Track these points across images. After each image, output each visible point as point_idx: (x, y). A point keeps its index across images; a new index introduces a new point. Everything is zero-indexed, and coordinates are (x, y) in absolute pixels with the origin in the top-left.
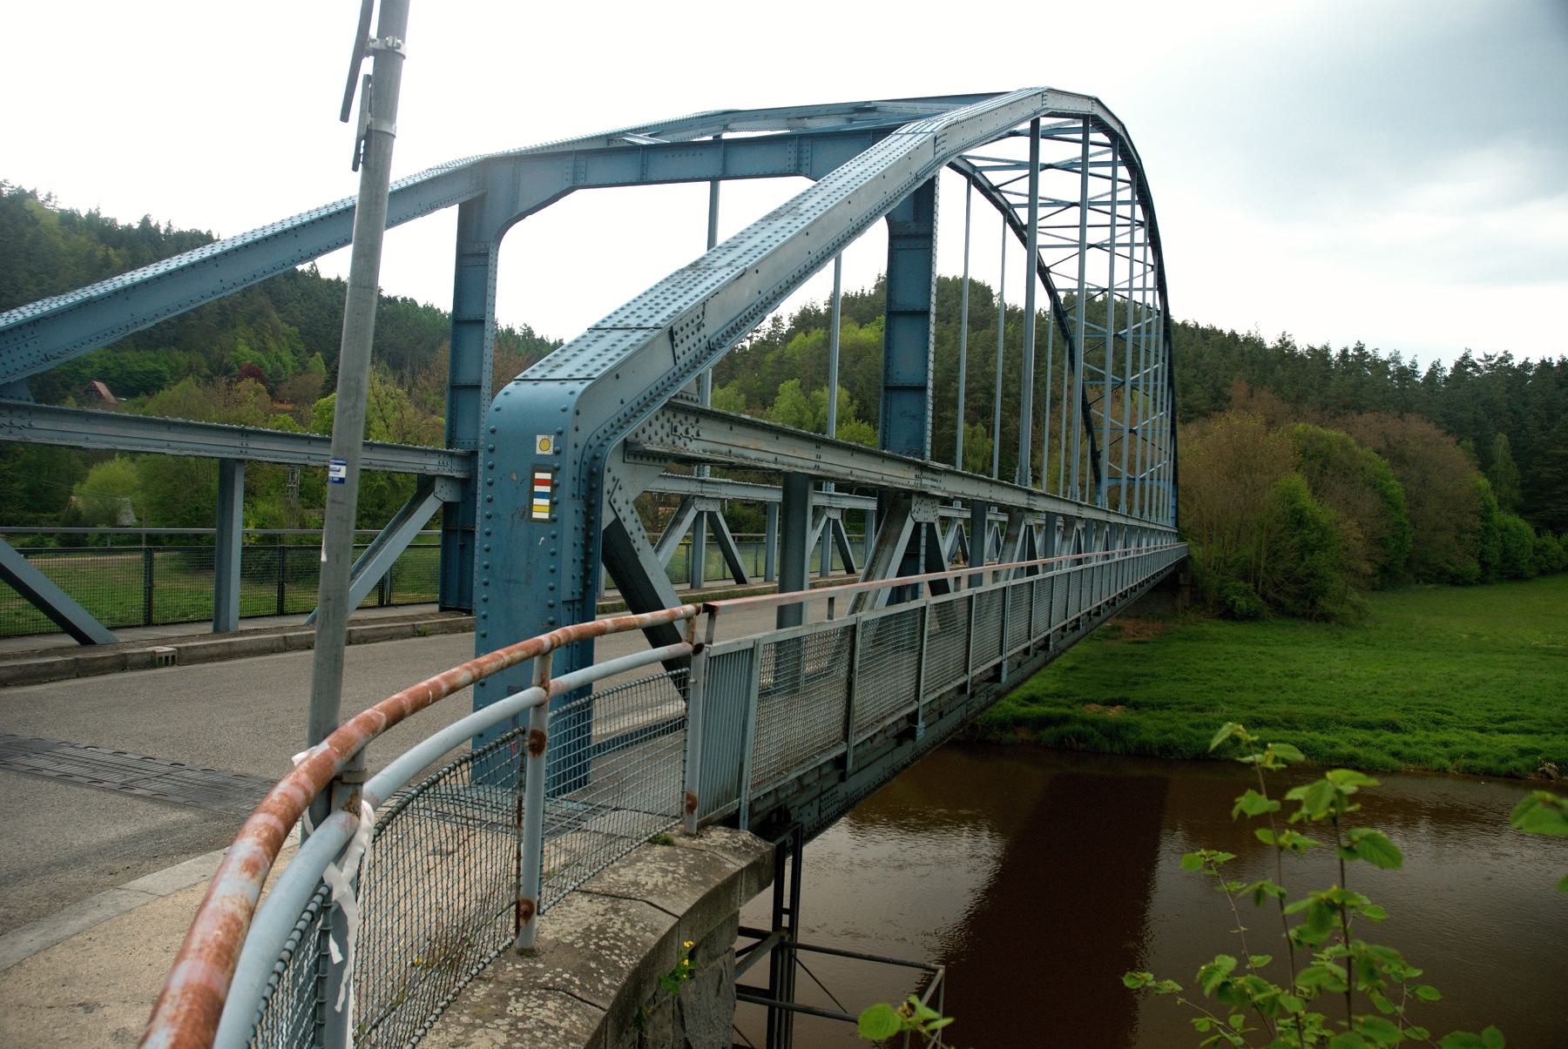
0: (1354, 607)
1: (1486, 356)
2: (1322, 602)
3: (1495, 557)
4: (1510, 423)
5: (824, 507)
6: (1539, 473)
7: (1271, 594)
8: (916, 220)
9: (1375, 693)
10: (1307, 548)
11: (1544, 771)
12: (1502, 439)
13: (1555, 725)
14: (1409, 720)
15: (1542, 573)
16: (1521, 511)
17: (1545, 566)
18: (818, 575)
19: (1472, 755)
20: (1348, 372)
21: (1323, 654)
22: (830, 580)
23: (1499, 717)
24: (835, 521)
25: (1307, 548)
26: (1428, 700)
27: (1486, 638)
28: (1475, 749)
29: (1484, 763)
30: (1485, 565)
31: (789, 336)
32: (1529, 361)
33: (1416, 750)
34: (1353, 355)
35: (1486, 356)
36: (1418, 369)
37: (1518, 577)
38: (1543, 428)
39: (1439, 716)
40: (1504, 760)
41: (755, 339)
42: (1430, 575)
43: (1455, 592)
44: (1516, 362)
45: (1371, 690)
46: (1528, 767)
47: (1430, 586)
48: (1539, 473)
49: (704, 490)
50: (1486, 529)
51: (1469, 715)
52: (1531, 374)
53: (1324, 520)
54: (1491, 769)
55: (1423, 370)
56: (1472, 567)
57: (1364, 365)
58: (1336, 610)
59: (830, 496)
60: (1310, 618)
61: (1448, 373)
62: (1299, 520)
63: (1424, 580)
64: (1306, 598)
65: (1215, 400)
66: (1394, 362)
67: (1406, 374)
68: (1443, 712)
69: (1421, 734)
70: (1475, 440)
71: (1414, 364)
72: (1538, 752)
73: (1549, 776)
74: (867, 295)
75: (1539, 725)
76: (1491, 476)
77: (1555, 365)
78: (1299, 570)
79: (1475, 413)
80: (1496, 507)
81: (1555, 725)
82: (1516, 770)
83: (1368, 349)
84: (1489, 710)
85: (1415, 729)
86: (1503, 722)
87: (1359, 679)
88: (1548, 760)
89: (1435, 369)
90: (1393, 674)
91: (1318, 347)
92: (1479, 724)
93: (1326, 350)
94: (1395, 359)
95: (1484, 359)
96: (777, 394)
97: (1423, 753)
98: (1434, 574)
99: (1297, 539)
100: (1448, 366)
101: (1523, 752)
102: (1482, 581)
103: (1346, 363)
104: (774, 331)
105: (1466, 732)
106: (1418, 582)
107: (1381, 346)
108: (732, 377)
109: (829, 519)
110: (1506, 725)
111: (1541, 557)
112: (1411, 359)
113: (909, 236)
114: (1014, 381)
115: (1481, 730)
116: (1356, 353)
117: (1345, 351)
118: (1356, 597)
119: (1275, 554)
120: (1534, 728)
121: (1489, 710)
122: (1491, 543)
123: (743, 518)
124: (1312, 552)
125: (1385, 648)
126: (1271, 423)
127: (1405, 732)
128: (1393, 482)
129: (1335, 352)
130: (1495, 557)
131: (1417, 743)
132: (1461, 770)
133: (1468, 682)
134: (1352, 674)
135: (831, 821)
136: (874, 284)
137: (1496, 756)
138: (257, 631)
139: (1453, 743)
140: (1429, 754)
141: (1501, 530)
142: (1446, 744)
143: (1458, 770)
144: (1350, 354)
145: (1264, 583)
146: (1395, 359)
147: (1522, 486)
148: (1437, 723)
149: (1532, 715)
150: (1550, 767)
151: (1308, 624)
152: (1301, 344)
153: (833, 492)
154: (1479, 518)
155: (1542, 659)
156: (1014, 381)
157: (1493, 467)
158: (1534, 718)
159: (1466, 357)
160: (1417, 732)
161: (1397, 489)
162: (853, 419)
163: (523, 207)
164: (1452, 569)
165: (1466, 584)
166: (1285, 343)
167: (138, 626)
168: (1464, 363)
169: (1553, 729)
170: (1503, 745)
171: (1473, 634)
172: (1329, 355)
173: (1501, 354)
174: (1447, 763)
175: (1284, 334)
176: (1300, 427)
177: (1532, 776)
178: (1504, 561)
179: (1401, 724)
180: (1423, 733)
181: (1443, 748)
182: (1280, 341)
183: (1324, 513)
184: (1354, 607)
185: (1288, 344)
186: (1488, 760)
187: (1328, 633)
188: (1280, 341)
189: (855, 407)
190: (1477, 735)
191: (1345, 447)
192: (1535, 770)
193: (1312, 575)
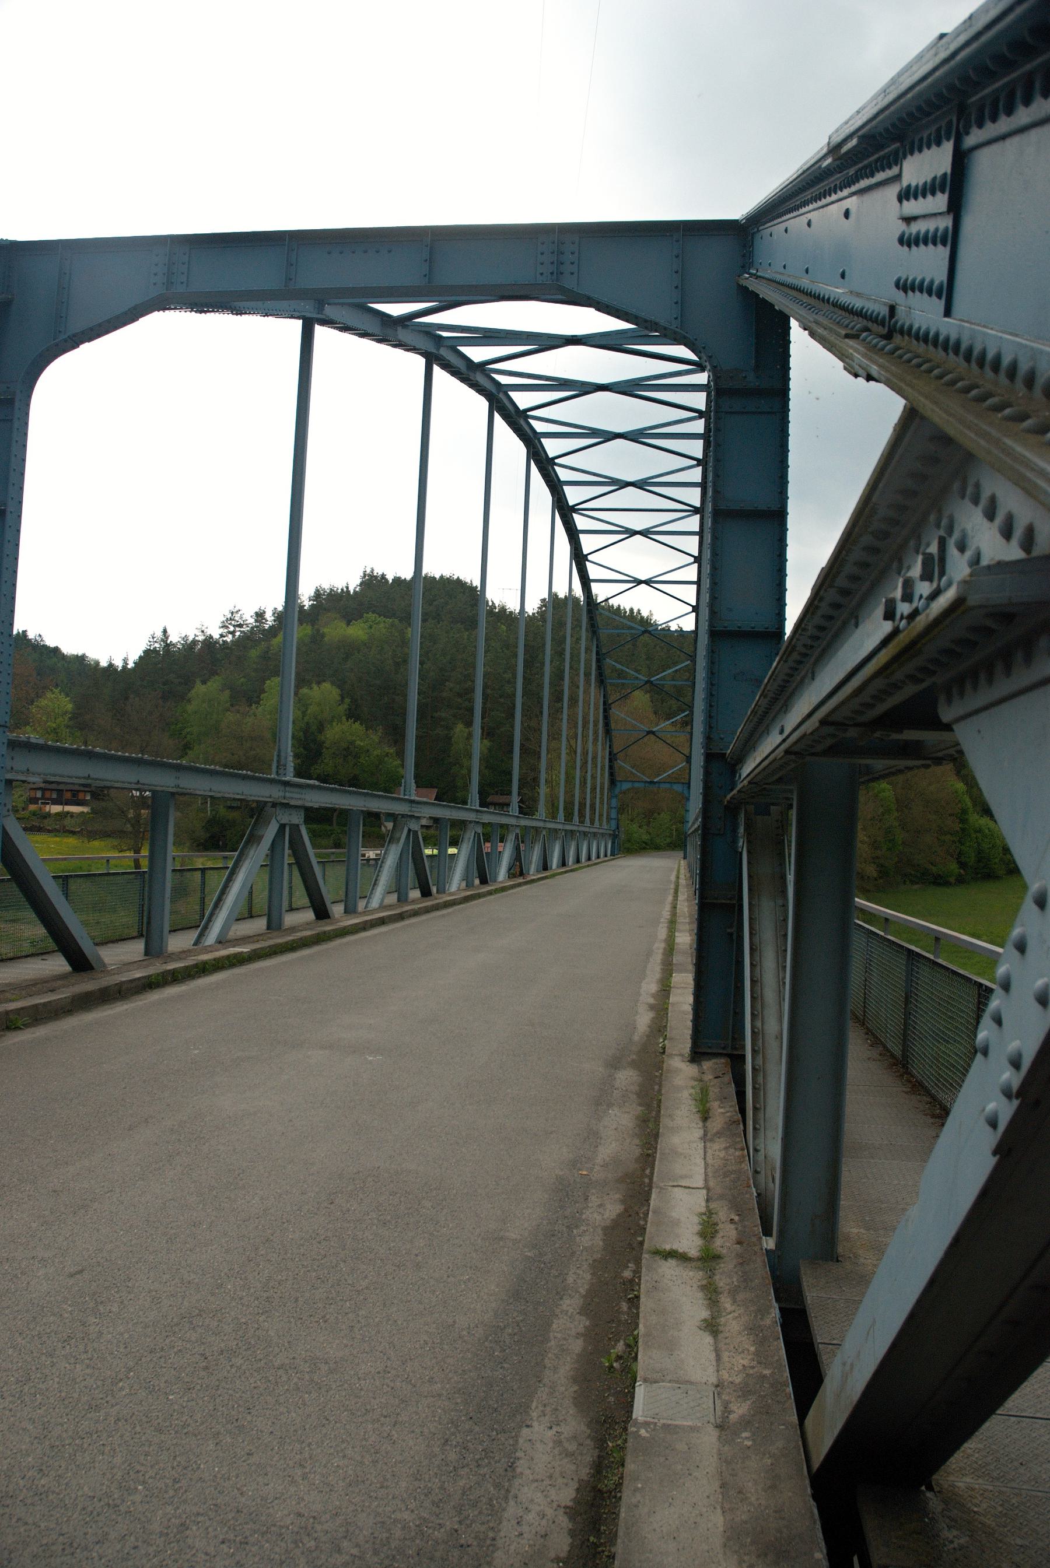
18: (259, 925)
24: (295, 828)
31: (273, 631)
41: (238, 634)
47: (916, 887)
49: (288, 795)
50: (963, 830)
74: (352, 592)
96: (263, 691)
102: (960, 881)
104: (256, 627)
108: (214, 673)
109: (409, 830)
114: (509, 682)
122: (968, 844)
123: (228, 821)
136: (359, 581)
138: (790, 855)
141: (976, 832)
153: (290, 777)
156: (509, 682)
162: (344, 718)
163: (77, 325)
164: (934, 869)
165: (947, 884)
167: (133, 938)
178: (979, 861)
189: (346, 706)
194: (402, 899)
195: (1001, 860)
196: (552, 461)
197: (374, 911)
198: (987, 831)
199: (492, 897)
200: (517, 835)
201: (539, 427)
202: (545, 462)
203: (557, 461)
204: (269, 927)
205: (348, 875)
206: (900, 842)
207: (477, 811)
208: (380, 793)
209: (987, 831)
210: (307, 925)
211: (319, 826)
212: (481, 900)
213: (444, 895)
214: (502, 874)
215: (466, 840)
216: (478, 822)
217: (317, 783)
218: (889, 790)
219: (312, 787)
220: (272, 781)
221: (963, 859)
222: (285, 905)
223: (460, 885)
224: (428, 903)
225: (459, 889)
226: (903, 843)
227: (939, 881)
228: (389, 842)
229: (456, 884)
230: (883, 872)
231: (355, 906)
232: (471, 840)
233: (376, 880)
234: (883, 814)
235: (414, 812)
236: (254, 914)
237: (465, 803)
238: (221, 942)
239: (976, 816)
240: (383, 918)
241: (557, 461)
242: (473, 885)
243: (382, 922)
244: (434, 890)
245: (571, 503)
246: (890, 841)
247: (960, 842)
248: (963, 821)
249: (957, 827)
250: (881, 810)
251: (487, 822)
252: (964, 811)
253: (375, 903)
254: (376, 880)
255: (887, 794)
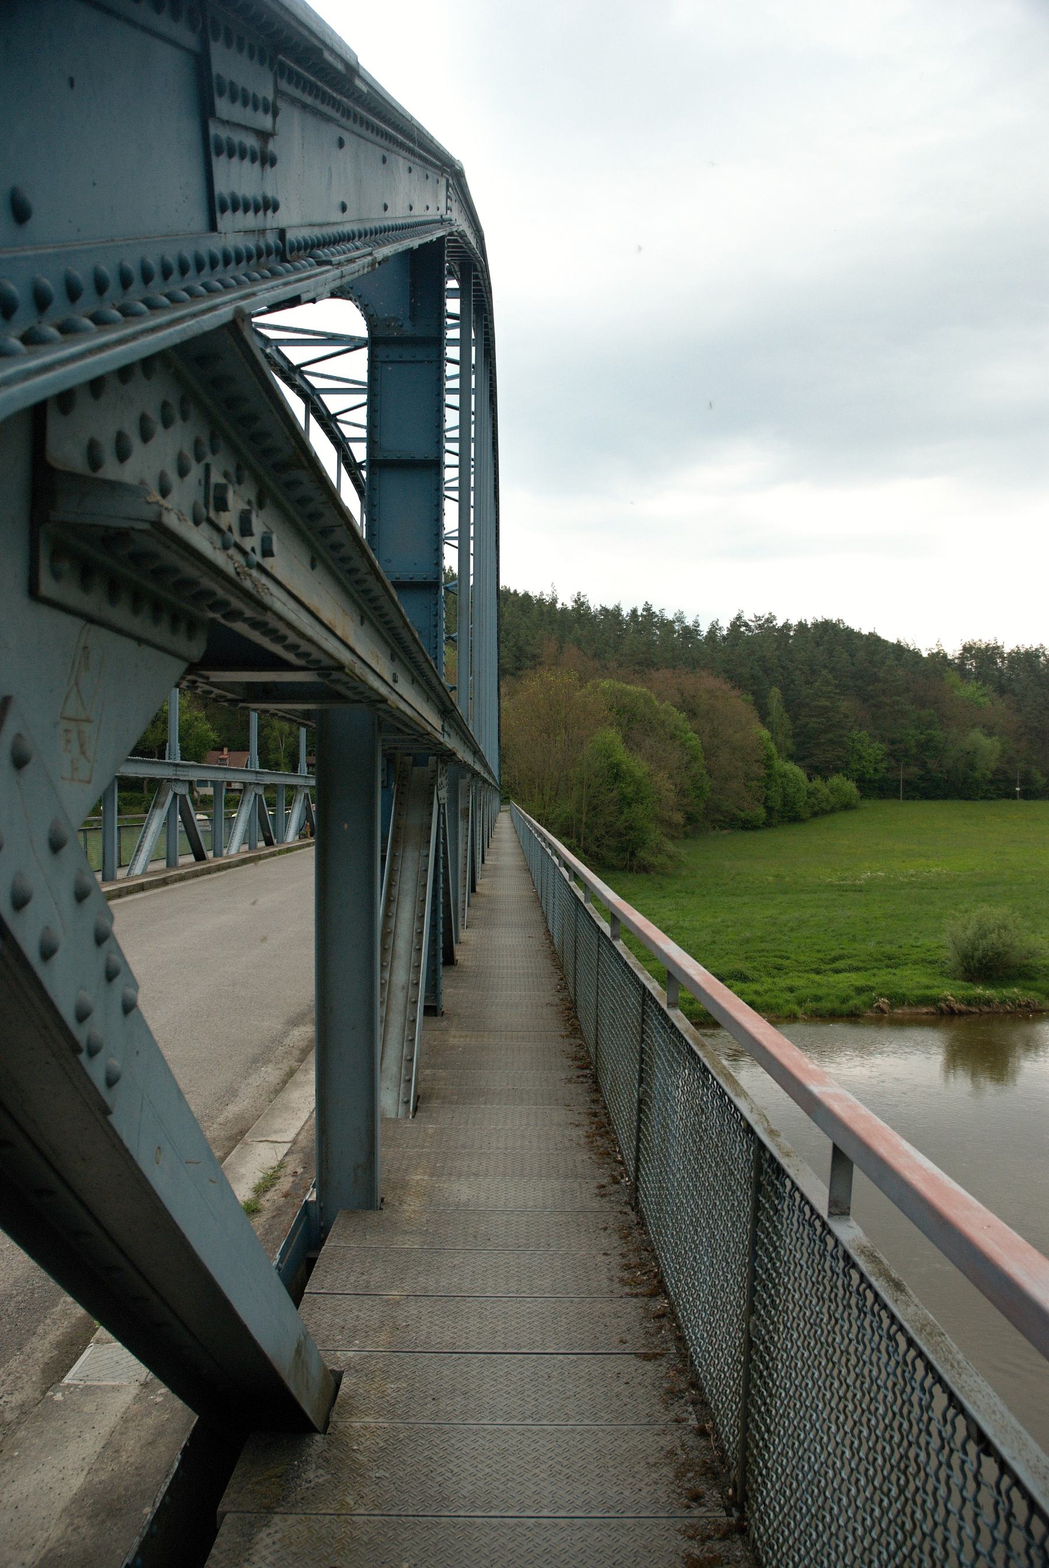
0: (670, 857)
1: (756, 617)
2: (642, 854)
3: (777, 803)
4: (781, 678)
5: (169, 780)
6: (807, 724)
7: (594, 848)
8: (413, 316)
9: (714, 942)
10: (625, 802)
11: (878, 1007)
12: (775, 692)
13: (876, 960)
14: (754, 968)
15: (815, 814)
16: (791, 757)
17: (816, 809)
18: (162, 864)
19: (817, 998)
20: (639, 632)
21: (651, 906)
22: (183, 871)
23: (829, 957)
25: (625, 802)
26: (763, 946)
27: (787, 879)
28: (820, 992)
29: (829, 1005)
30: (769, 810)
32: (789, 622)
33: (766, 998)
34: (642, 615)
35: (756, 617)
36: (701, 628)
37: (795, 819)
38: (807, 682)
39: (780, 961)
40: (845, 1000)
42: (724, 822)
43: (749, 835)
44: (779, 623)
45: (709, 939)
46: (865, 1003)
47: (725, 832)
48: (807, 724)
49: (178, 773)
51: (802, 958)
52: (792, 633)
53: (639, 773)
54: (834, 1009)
55: (704, 629)
56: (759, 812)
57: (654, 624)
58: (651, 859)
59: (177, 765)
60: (631, 870)
61: (725, 632)
62: (616, 774)
63: (720, 827)
64: (625, 850)
65: (518, 658)
66: (678, 621)
67: (690, 633)
68: (782, 957)
69: (767, 982)
70: (753, 694)
71: (697, 624)
72: (871, 989)
73: (883, 1011)
75: (864, 961)
76: (768, 726)
77: (809, 626)
78: (618, 823)
79: (752, 668)
80: (776, 756)
81: (876, 960)
82: (857, 1008)
83: (655, 609)
84: (819, 951)
85: (761, 977)
86: (834, 962)
87: (694, 929)
88: (881, 995)
89: (714, 629)
90: (723, 922)
91: (610, 607)
92: (814, 966)
93: (618, 609)
94: (680, 619)
95: (754, 619)
97: (774, 1001)
98: (727, 820)
99: (615, 792)
100: (725, 624)
101: (860, 990)
102: (767, 825)
103: (636, 622)
105: (806, 975)
106: (714, 828)
107: (667, 607)
109: (175, 795)
110: (839, 965)
111: (813, 799)
112: (694, 619)
113: (401, 341)
115: (818, 972)
116: (645, 613)
117: (634, 611)
118: (670, 846)
119: (595, 809)
120: (861, 965)
121: (819, 951)
124: (629, 805)
125: (704, 896)
126: (582, 680)
127: (753, 981)
128: (690, 734)
129: (626, 612)
130: (777, 803)
131: (766, 992)
132: (809, 1013)
133: (791, 924)
134: (686, 924)
135: (78, 1060)
137: (837, 997)
139: (798, 988)
140: (781, 1001)
141: (781, 776)
142: (791, 990)
143: (806, 1014)
144: (639, 614)
145: (585, 839)
146: (680, 619)
147: (794, 736)
148: (779, 968)
149: (855, 952)
150: (884, 1002)
151: (630, 876)
152: (595, 604)
153: (178, 761)
154: (763, 766)
155: (841, 896)
157: (769, 719)
158: (859, 956)
159: (739, 618)
160: (763, 979)
161: (695, 741)
164: (743, 815)
165: (755, 828)
166: (580, 603)
168: (737, 623)
169: (876, 964)
170: (841, 985)
171: (777, 876)
172: (620, 615)
173: (767, 616)
174: (795, 1008)
175: (579, 594)
176: (605, 684)
177: (869, 1014)
178: (785, 805)
179: (748, 973)
180: (770, 980)
181: (789, 994)
182: (576, 601)
183: (637, 765)
184: (670, 857)
185: (583, 603)
186: (831, 1001)
187: (650, 884)
188: (576, 601)
190: (817, 978)
191: (648, 701)
192: (871, 1006)
193: (631, 828)
194: (171, 864)
195: (806, 803)
196: (333, 418)
197: (138, 877)
198: (791, 776)
199: (274, 858)
200: (306, 796)
201: (317, 383)
202: (326, 418)
203: (338, 417)
204: (168, 866)
205: (104, 840)
206: (708, 790)
207: (257, 772)
208: (192, 763)
209: (791, 776)
210: (191, 865)
211: (130, 794)
212: (230, 870)
213: (219, 859)
214: (291, 835)
215: (298, 801)
216: (258, 784)
217: (196, 763)
218: (696, 739)
219: (192, 766)
220: (169, 764)
221: (770, 804)
222: (116, 864)
223: (239, 848)
224: (272, 849)
225: (238, 852)
226: (712, 790)
227: (748, 826)
228: (154, 807)
229: (235, 847)
230: (690, 819)
231: (113, 874)
232: (251, 802)
233: (140, 846)
234: (690, 762)
235: (178, 775)
236: (122, 864)
237: (162, 756)
238: (145, 873)
239: (781, 762)
240: (142, 884)
241: (338, 417)
242: (256, 847)
243: (142, 888)
244: (275, 841)
245: (358, 461)
246: (698, 788)
247: (766, 787)
248: (769, 767)
249: (763, 772)
250: (686, 758)
251: (268, 783)
252: (769, 758)
253: (138, 870)
254: (140, 846)
255: (694, 743)
